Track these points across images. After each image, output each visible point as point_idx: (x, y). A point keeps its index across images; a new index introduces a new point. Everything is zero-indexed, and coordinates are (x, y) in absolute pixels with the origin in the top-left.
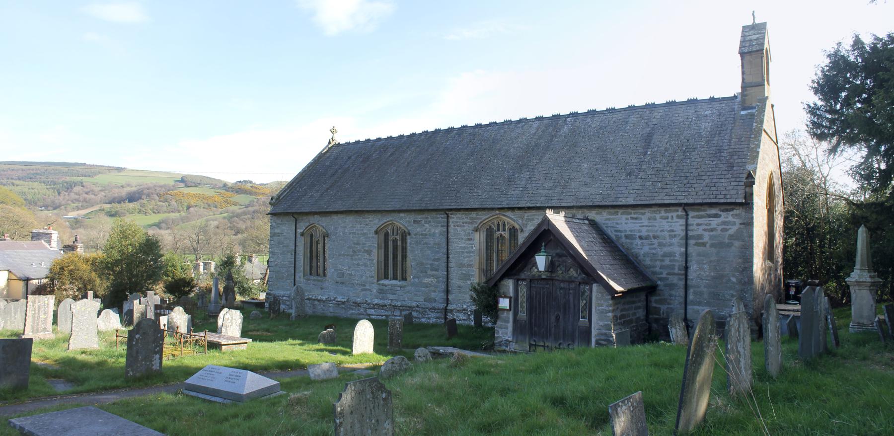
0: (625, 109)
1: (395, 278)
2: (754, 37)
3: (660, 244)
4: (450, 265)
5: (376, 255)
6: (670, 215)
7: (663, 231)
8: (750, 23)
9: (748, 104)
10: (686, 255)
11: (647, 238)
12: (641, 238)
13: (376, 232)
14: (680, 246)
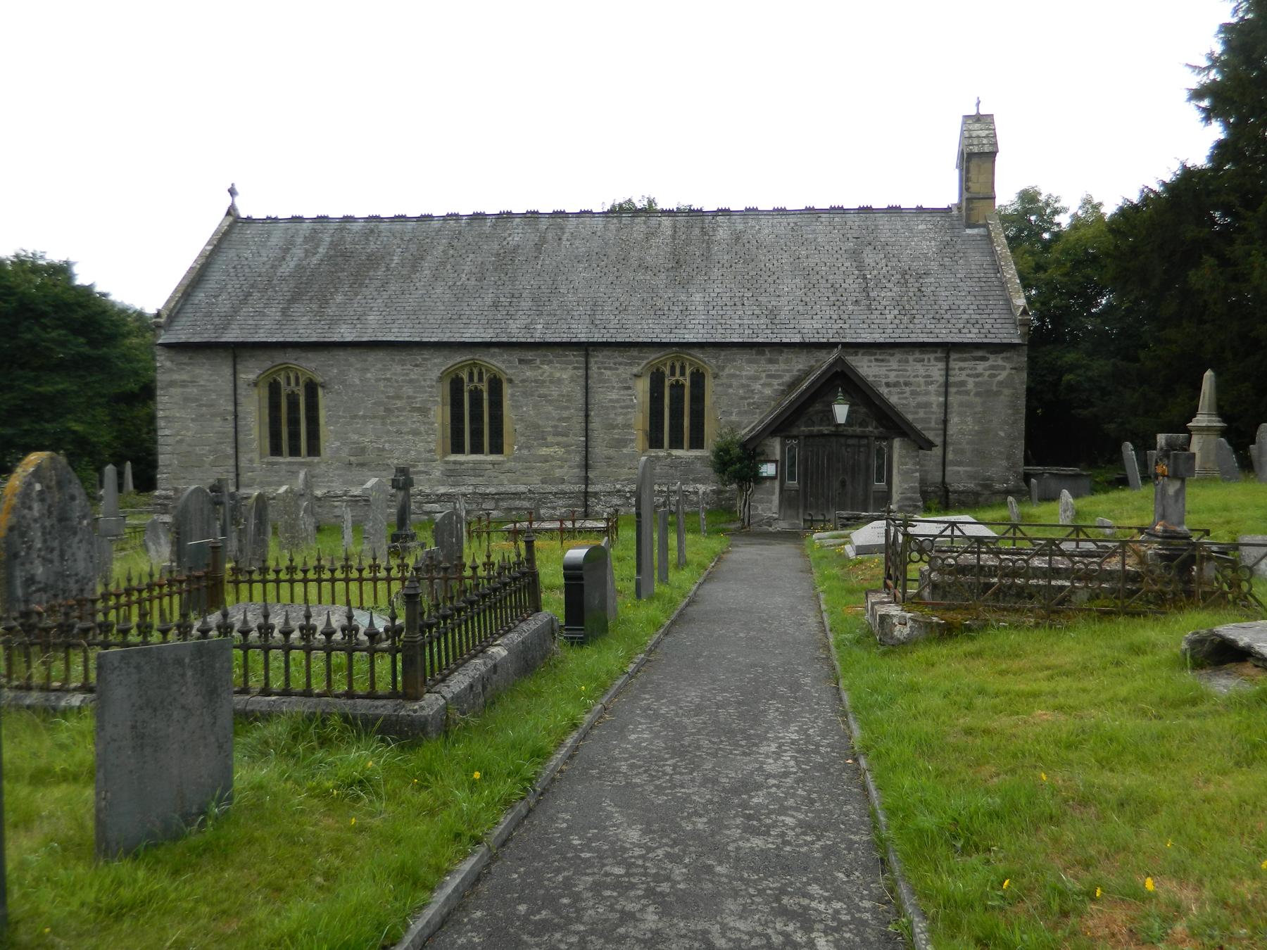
0: (800, 212)
1: (477, 449)
2: (983, 133)
3: (913, 393)
4: (591, 426)
5: (440, 415)
6: (926, 357)
7: (917, 376)
8: (974, 113)
9: (973, 220)
10: (946, 405)
11: (896, 385)
12: (888, 385)
13: (440, 379)
14: (939, 395)
